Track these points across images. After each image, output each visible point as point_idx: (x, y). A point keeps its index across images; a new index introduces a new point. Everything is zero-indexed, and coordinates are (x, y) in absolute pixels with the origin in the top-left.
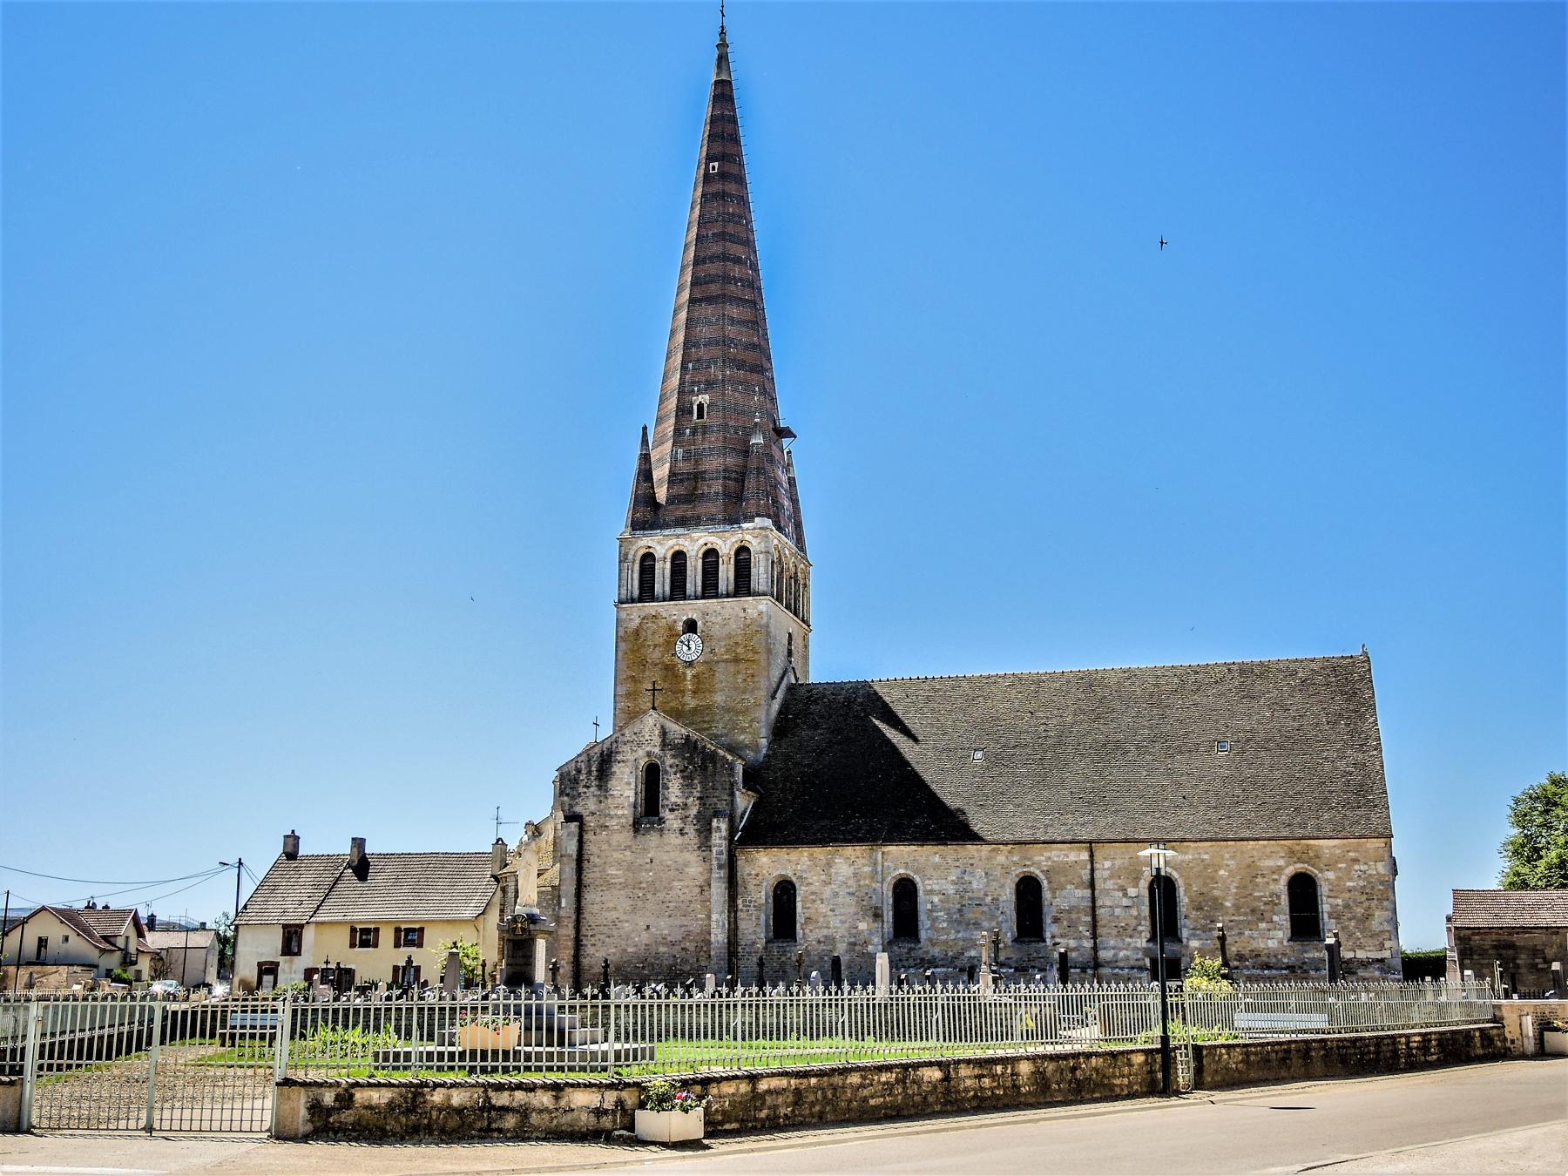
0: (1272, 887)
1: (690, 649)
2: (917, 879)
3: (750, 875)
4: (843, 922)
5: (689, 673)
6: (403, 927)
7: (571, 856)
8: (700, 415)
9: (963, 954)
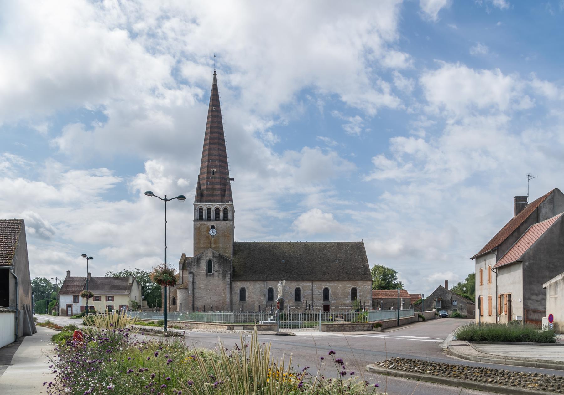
1: (212, 232)
2: (274, 288)
7: (191, 281)
8: (213, 174)
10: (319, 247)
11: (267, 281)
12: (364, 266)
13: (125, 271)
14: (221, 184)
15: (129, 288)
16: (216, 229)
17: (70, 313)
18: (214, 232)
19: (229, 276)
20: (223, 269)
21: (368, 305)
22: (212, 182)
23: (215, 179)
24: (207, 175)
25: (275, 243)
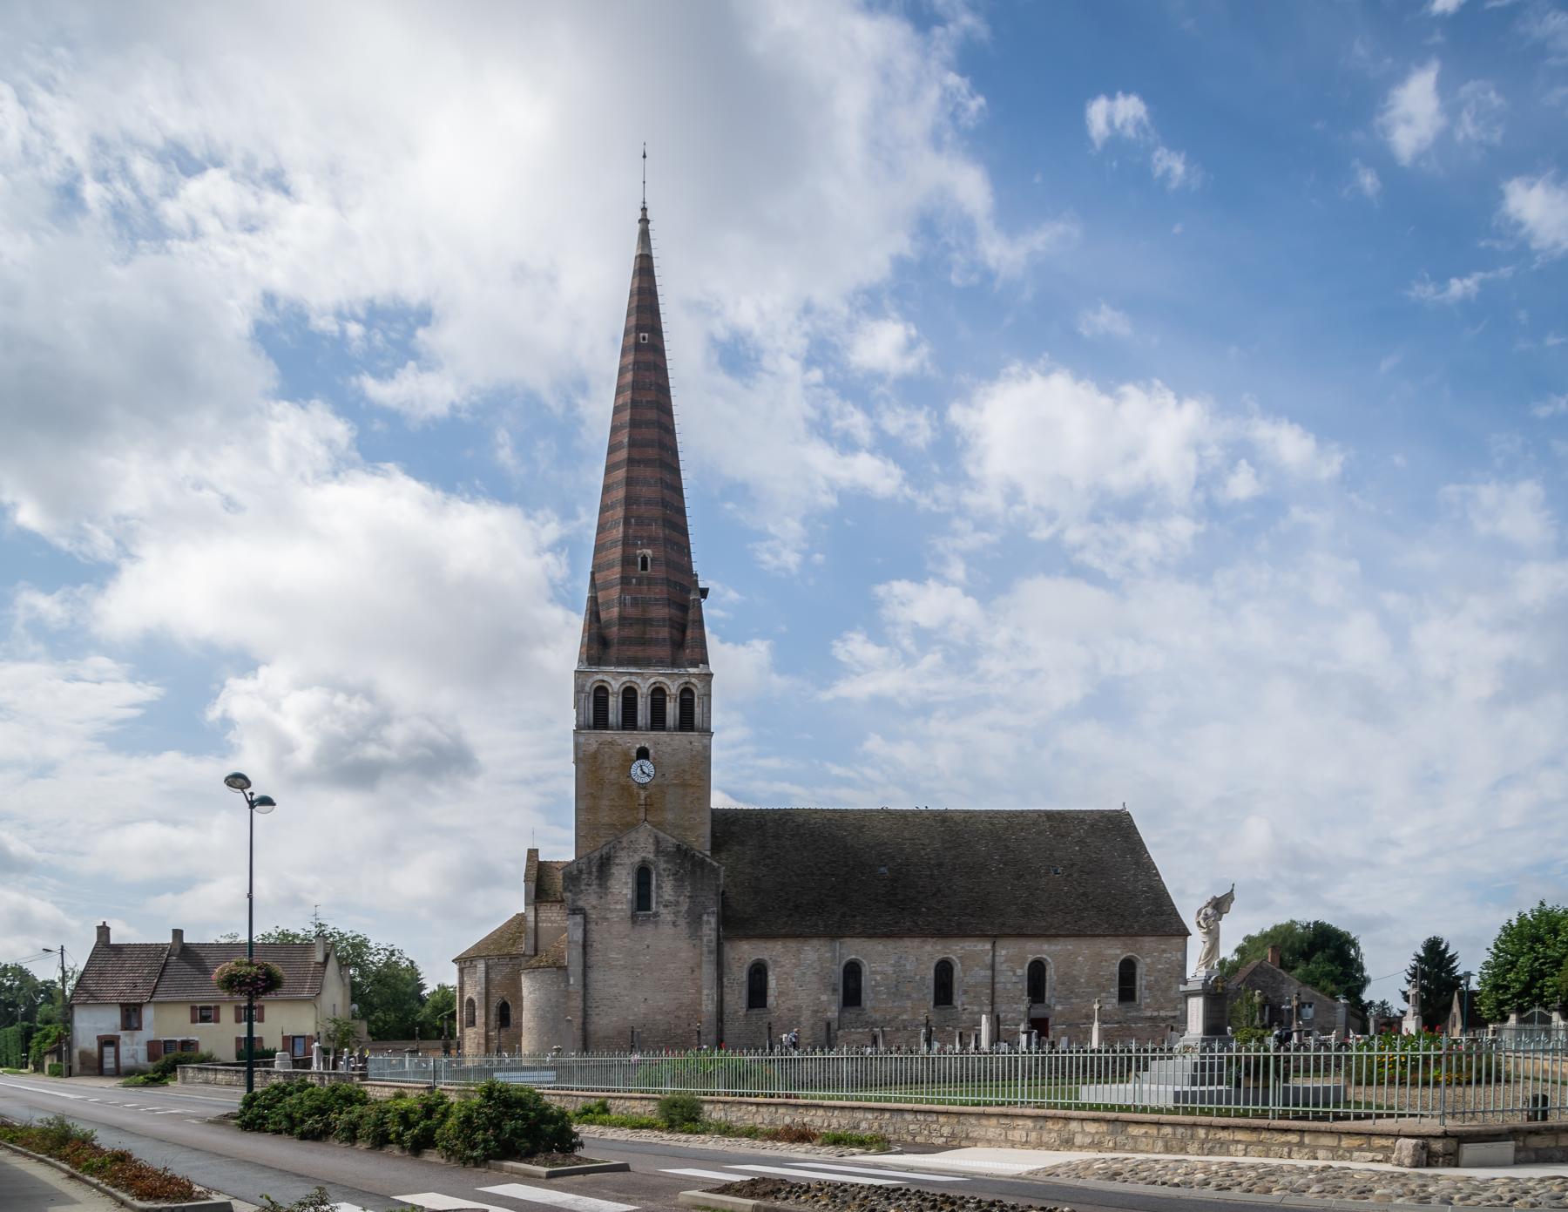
0: (1111, 969)
1: (641, 772)
3: (734, 959)
4: (809, 995)
5: (643, 794)
6: (198, 1005)
7: (578, 942)
8: (644, 567)
9: (897, 1018)
10: (990, 827)
11: (842, 937)
12: (1151, 887)
13: (279, 930)
14: (670, 602)
15: (314, 977)
16: (654, 759)
17: (113, 1066)
18: (646, 771)
19: (713, 920)
20: (689, 897)
21: (1174, 1017)
22: (639, 596)
23: (649, 584)
24: (623, 571)
25: (843, 814)
